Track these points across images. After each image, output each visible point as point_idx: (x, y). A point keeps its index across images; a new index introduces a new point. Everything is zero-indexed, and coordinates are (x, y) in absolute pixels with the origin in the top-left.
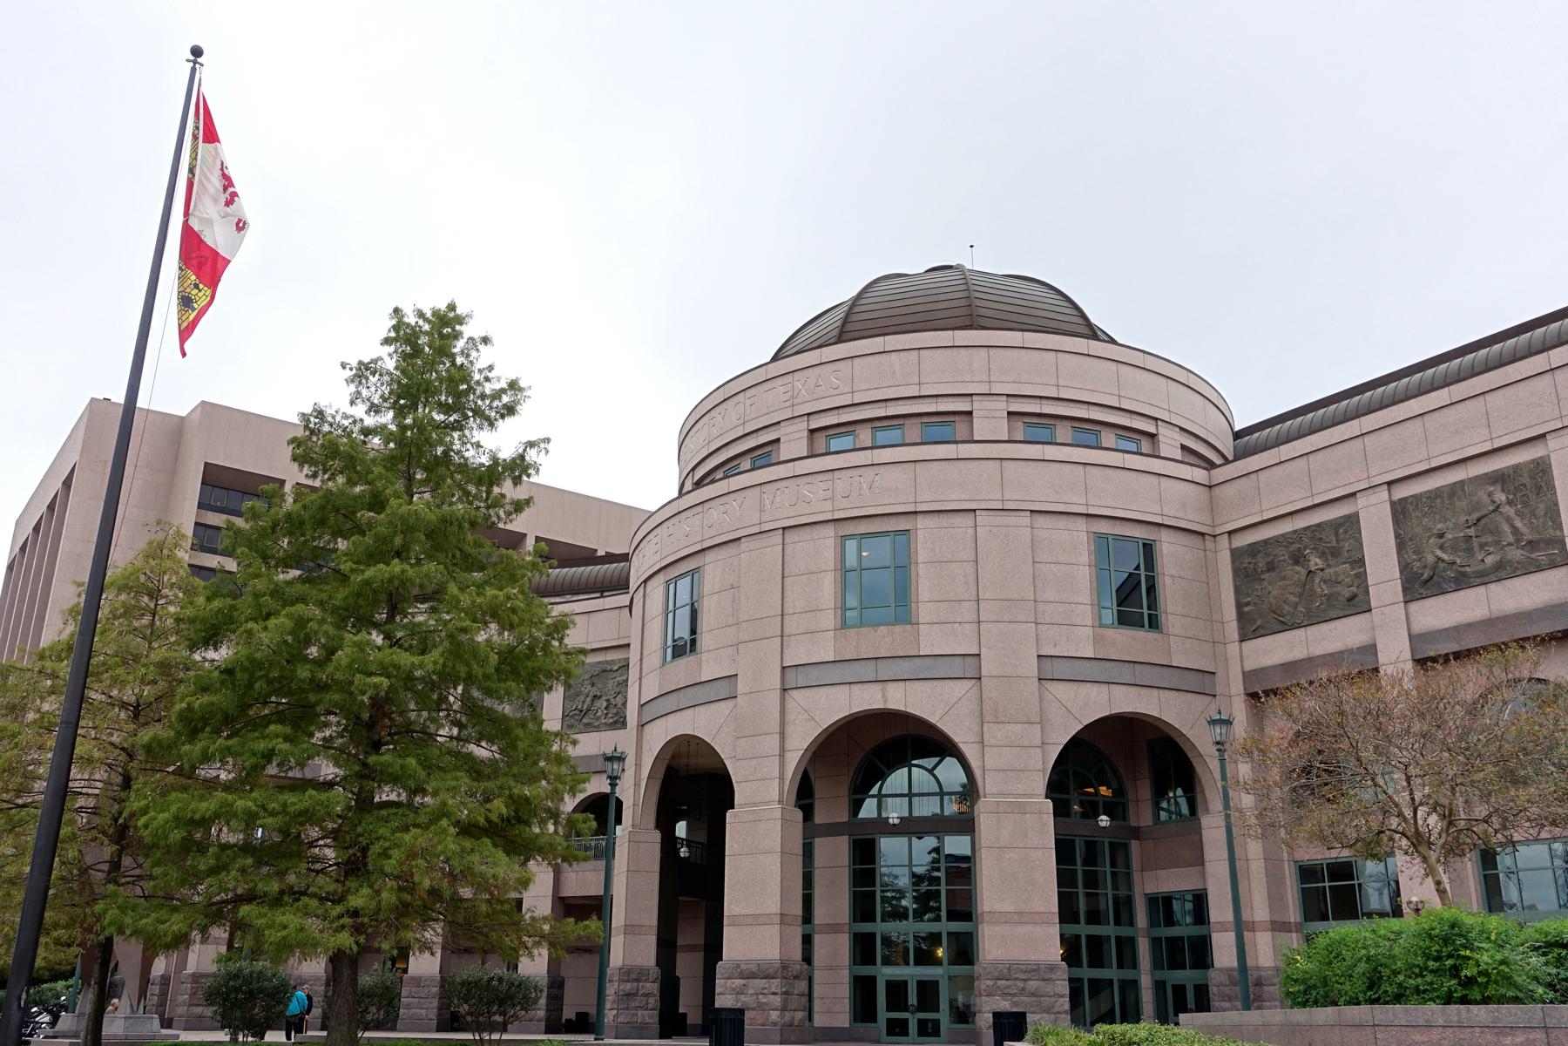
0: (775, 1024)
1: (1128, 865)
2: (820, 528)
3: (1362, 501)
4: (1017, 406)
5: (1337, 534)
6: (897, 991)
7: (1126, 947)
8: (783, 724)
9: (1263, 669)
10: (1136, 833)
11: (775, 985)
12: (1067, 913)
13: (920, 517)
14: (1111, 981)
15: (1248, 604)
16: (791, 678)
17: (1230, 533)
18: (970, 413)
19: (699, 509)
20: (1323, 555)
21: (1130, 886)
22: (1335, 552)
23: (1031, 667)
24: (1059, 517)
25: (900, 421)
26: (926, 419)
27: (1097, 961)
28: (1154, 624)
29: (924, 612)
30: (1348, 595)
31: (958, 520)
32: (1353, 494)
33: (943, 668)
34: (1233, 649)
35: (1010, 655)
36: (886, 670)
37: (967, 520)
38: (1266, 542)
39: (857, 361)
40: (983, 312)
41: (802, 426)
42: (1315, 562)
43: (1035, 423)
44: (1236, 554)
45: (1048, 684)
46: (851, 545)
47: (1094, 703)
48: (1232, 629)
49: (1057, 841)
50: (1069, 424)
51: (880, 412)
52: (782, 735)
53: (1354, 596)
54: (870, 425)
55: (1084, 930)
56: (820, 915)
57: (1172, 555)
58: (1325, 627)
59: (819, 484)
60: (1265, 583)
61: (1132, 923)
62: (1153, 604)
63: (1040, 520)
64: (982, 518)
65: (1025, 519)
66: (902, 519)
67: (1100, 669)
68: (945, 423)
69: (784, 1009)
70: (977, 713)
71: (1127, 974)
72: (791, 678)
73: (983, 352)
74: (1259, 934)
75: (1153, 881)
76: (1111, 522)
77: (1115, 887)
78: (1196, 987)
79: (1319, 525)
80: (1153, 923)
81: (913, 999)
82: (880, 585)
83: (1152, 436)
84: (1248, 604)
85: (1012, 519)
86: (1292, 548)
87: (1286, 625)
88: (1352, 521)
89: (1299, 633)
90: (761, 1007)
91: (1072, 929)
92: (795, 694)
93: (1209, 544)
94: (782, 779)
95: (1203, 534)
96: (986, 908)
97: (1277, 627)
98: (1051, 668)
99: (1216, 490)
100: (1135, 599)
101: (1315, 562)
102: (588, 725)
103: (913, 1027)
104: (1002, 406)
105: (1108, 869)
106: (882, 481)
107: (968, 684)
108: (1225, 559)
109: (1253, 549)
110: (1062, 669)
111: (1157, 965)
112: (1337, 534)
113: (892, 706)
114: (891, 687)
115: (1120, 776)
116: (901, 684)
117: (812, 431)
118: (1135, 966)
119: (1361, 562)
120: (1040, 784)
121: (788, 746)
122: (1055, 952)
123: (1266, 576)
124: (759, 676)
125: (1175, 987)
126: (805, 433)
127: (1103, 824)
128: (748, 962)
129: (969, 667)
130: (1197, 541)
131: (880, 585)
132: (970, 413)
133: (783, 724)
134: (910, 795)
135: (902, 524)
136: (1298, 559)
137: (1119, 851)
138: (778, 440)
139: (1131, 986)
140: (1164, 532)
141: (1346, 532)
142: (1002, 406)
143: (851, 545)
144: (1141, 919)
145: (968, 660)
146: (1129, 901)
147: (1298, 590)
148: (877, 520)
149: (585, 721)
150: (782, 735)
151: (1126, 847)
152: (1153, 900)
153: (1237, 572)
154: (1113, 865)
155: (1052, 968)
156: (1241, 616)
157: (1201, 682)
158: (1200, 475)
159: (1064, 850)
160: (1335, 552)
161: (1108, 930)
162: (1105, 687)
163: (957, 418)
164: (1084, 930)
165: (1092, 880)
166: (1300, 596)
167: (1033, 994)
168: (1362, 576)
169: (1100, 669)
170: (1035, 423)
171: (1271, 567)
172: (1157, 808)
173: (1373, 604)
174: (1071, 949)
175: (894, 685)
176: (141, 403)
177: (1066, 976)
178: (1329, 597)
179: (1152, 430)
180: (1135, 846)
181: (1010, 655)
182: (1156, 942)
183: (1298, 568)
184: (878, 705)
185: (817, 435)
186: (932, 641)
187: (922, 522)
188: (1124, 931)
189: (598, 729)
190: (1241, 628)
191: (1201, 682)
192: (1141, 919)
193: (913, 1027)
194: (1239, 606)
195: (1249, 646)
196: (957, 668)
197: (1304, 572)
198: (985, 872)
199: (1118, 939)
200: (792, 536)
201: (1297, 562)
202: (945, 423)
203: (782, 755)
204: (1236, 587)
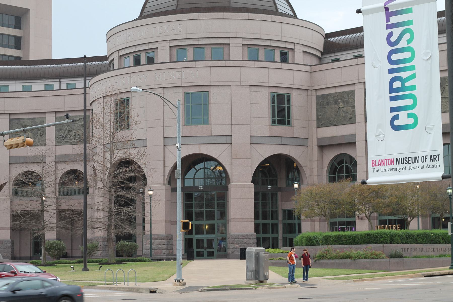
0: (164, 254)
1: (277, 200)
2: (177, 89)
3: (47, 115)
4: (245, 42)
5: (348, 96)
6: (199, 242)
7: (275, 226)
10: (280, 189)
11: (164, 242)
12: (257, 216)
15: (320, 115)
16: (168, 141)
18: (229, 44)
20: (344, 102)
21: (277, 208)
22: (347, 102)
24: (259, 87)
25: (204, 46)
27: (265, 231)
28: (289, 123)
29: (213, 121)
30: (349, 117)
33: (219, 140)
35: (241, 136)
36: (200, 140)
37: (230, 87)
41: (167, 44)
42: (341, 105)
43: (255, 51)
44: (317, 97)
45: (253, 145)
46: (174, 50)
47: (267, 151)
48: (315, 123)
49: (254, 193)
50: (263, 47)
52: (164, 161)
53: (351, 118)
54: (192, 47)
55: (261, 221)
56: (149, 214)
57: (297, 101)
59: (176, 72)
60: (326, 109)
62: (289, 116)
63: (253, 88)
65: (248, 88)
67: (270, 139)
68: (217, 50)
69: (167, 249)
70: (230, 155)
71: (275, 235)
72: (168, 141)
73: (234, 21)
75: (283, 206)
76: (277, 88)
77: (272, 208)
78: (289, 239)
79: (343, 92)
81: (205, 245)
82: (196, 105)
83: (293, 50)
84: (320, 115)
85: (243, 88)
86: (335, 98)
88: (353, 92)
90: (159, 249)
91: (258, 222)
93: (309, 93)
94: (164, 176)
97: (328, 125)
98: (255, 140)
99: (313, 73)
100: (281, 111)
102: (67, 142)
103: (205, 254)
104: (241, 42)
105: (270, 202)
106: (197, 74)
107: (228, 145)
109: (323, 96)
110: (259, 140)
111: (284, 232)
112: (348, 96)
113: (202, 152)
115: (275, 173)
116: (205, 145)
117: (170, 47)
118: (277, 232)
119: (354, 107)
120: (250, 178)
121: (166, 165)
122: (251, 229)
124: (155, 140)
125: (289, 239)
126: (168, 48)
129: (227, 139)
130: (305, 92)
131: (196, 105)
132: (229, 44)
134: (194, 179)
135: (206, 89)
136: (336, 102)
137: (274, 195)
139: (276, 239)
140: (294, 90)
141: (351, 96)
142: (241, 42)
143: (174, 50)
144: (280, 217)
145: (228, 137)
146: (277, 211)
147: (336, 113)
148: (198, 87)
149: (66, 140)
150: (164, 161)
151: (276, 194)
152: (284, 211)
153: (317, 103)
155: (252, 235)
156: (318, 119)
157: (303, 142)
158: (308, 68)
159: (256, 194)
160: (347, 102)
161: (269, 222)
162: (272, 145)
163: (224, 46)
164: (261, 221)
165: (264, 205)
166: (336, 115)
167: (246, 243)
169: (270, 139)
170: (255, 51)
171: (328, 104)
174: (257, 227)
175: (203, 145)
176: (82, 146)
178: (344, 117)
180: (279, 194)
181: (241, 136)
182: (284, 225)
183: (336, 106)
184: (197, 152)
186: (216, 130)
187: (213, 89)
188: (274, 222)
189: (71, 144)
190: (317, 123)
191: (303, 142)
192: (280, 217)
193: (205, 254)
194: (317, 116)
195: (320, 129)
196: (224, 140)
197: (338, 107)
198: (232, 197)
199: (272, 225)
200: (165, 89)
201: (336, 104)
202: (217, 50)
204: (317, 109)
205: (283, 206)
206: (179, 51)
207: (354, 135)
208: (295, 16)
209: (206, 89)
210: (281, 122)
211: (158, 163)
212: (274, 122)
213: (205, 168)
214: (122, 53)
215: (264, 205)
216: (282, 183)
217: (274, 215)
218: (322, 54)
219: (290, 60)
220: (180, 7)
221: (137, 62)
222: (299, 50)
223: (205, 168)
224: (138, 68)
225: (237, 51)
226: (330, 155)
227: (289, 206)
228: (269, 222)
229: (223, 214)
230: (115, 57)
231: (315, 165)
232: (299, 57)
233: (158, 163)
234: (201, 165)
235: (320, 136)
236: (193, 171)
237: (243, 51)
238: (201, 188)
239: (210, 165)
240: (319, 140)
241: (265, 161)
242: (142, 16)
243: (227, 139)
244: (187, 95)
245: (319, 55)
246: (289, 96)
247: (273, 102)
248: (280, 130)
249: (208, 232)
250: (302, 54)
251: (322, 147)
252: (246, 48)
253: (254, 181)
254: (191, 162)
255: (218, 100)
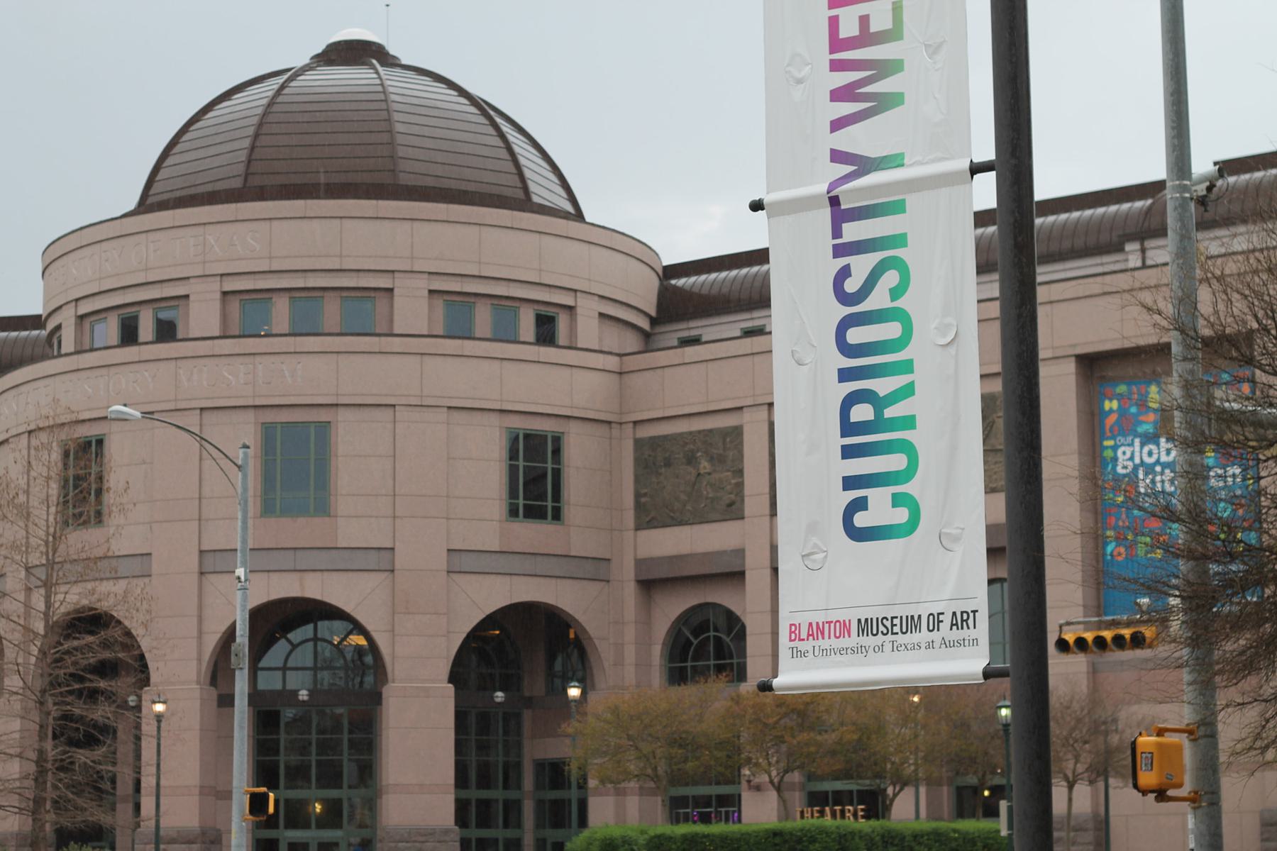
5: (724, 443)
7: (512, 812)
8: (200, 607)
9: (652, 559)
10: (529, 702)
12: (461, 779)
13: (341, 410)
14: (497, 840)
15: (645, 495)
17: (635, 423)
18: (391, 290)
19: (104, 371)
20: (711, 459)
21: (519, 755)
23: (441, 561)
26: (345, 294)
27: (484, 822)
28: (557, 516)
29: (343, 505)
31: (377, 413)
32: (741, 408)
34: (631, 533)
35: (421, 549)
37: (390, 411)
38: (665, 437)
39: (275, 223)
40: (411, 152)
41: (215, 287)
42: (705, 465)
43: (463, 310)
44: (638, 443)
45: (455, 576)
48: (630, 517)
50: (489, 301)
51: (299, 282)
54: (287, 295)
58: (706, 527)
61: (519, 787)
62: (557, 496)
63: (455, 414)
64: (401, 413)
65: (442, 415)
66: (323, 411)
68: (359, 307)
71: (510, 833)
72: (211, 562)
73: (407, 225)
74: (628, 798)
75: (537, 749)
76: (522, 417)
79: (711, 431)
80: (539, 786)
82: (295, 461)
84: (645, 495)
87: (676, 520)
88: (737, 432)
89: (686, 530)
91: (465, 794)
92: (212, 578)
93: (615, 431)
94: (199, 660)
95: (610, 423)
96: (391, 782)
98: (461, 561)
99: (625, 376)
100: (535, 479)
101: (705, 465)
104: (423, 284)
106: (299, 373)
108: (629, 446)
109: (655, 442)
111: (539, 825)
112: (724, 443)
114: (310, 577)
115: (516, 657)
117: (225, 293)
118: (519, 825)
119: (740, 472)
120: (444, 668)
123: (663, 470)
126: (218, 296)
127: (498, 700)
128: (778, 810)
129: (381, 559)
130: (603, 429)
131: (295, 461)
133: (200, 607)
134: (284, 669)
135: (322, 416)
136: (691, 460)
137: (511, 718)
138: (187, 296)
141: (731, 442)
144: (528, 781)
146: (518, 765)
151: (518, 716)
152: (540, 765)
153: (637, 461)
154: (506, 733)
155: (446, 832)
156: (639, 507)
157: (595, 569)
159: (460, 717)
161: (497, 794)
164: (474, 794)
168: (740, 485)
170: (463, 310)
171: (668, 464)
172: (551, 659)
173: (747, 513)
174: (461, 811)
175: (311, 575)
177: (458, 838)
179: (570, 302)
180: (527, 715)
181: (421, 549)
182: (540, 803)
183: (690, 469)
185: (229, 297)
187: (343, 414)
188: (512, 795)
191: (595, 569)
192: (528, 781)
194: (638, 496)
195: (643, 534)
197: (694, 472)
200: (206, 415)
202: (359, 307)
203: (200, 633)
205: (537, 749)
206: (248, 309)
207: (740, 553)
208: (579, 216)
209: (322, 416)
210: (535, 513)
211: (181, 624)
212: (513, 512)
213: (315, 639)
214: (85, 308)
215: (483, 747)
216: (535, 685)
217: (511, 775)
218: (654, 322)
219: (562, 338)
220: (255, 181)
221: (129, 335)
222: (588, 310)
223: (315, 639)
224: (130, 352)
225: (413, 309)
226: (672, 608)
227: (553, 749)
228: (497, 794)
229: (367, 771)
230: (67, 319)
231: (630, 633)
232: (588, 329)
233: (181, 624)
234: (307, 631)
235: (643, 553)
236: (281, 648)
237: (431, 307)
238: (303, 695)
239: (332, 631)
240: (640, 563)
241: (490, 621)
242: (146, 204)
243: (381, 559)
244: (268, 432)
245: (644, 324)
246: (557, 440)
247: (513, 455)
248: (531, 534)
249: (323, 822)
250: (595, 322)
251: (651, 585)
252: (439, 303)
253: (456, 676)
254: (276, 621)
255: (354, 444)
